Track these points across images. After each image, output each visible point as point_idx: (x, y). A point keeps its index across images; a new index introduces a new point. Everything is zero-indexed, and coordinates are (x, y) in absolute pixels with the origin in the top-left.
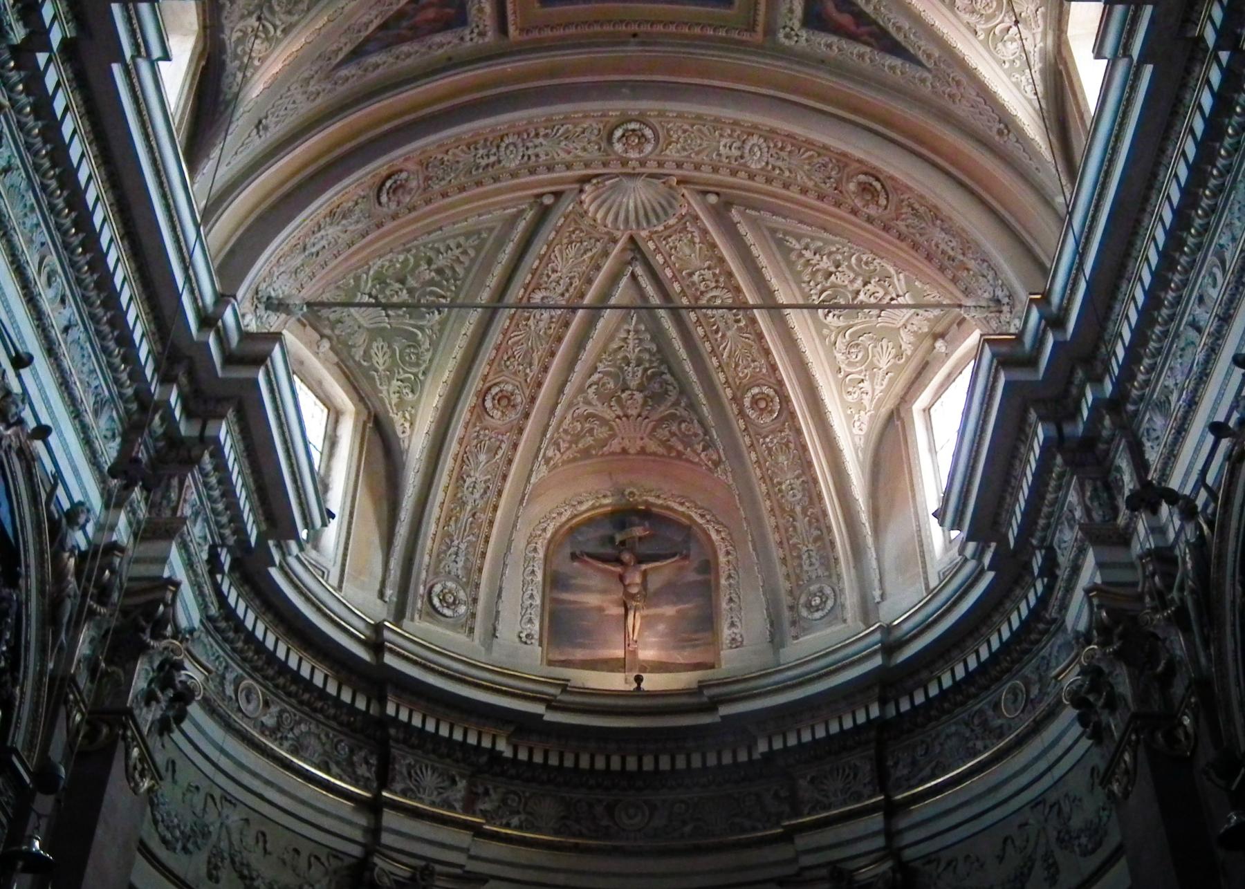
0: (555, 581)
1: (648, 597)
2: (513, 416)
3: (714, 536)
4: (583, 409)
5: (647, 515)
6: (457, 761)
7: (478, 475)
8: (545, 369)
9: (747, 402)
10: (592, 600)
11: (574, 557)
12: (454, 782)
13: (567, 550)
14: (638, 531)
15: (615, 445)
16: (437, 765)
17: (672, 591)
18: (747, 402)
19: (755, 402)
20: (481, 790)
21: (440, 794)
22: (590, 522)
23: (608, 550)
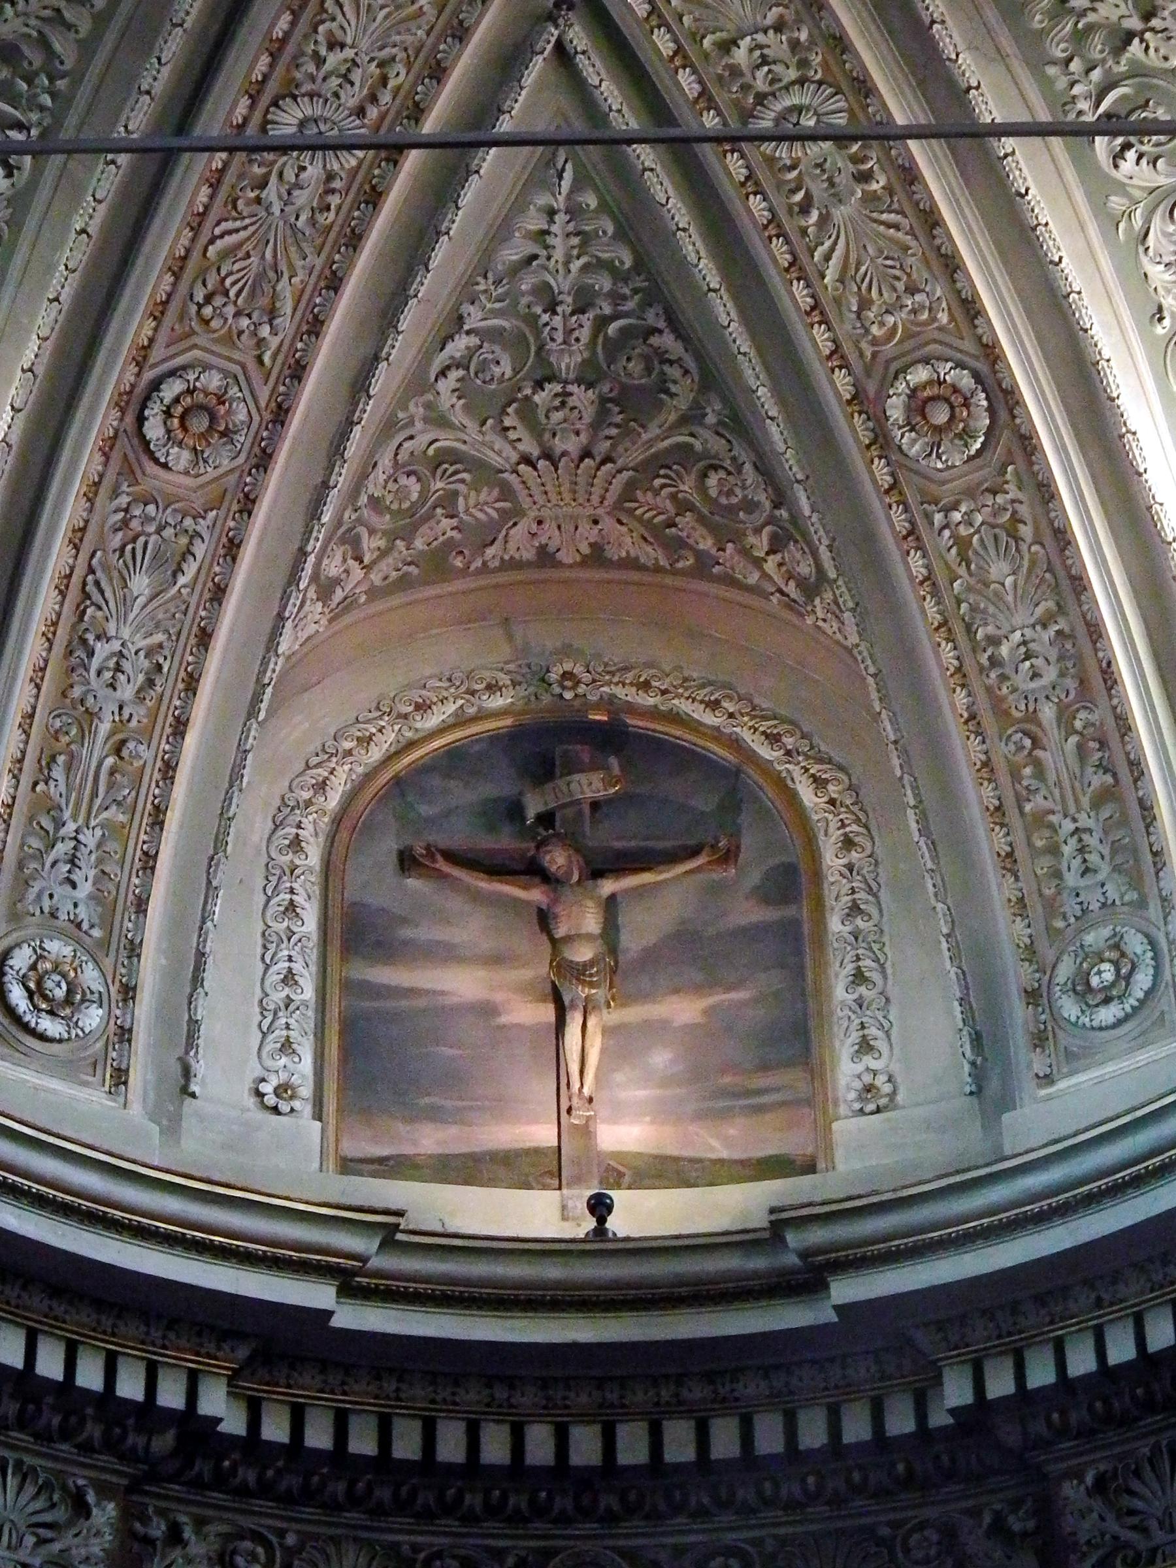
0: (355, 932)
1: (618, 971)
2: (224, 461)
3: (807, 794)
4: (423, 438)
5: (611, 738)
6: (86, 1448)
7: (127, 635)
8: (315, 326)
9: (896, 409)
10: (462, 984)
11: (407, 862)
12: (81, 1509)
13: (388, 845)
14: (589, 786)
15: (519, 541)
16: (29, 1460)
17: (692, 954)
18: (896, 409)
19: (918, 404)
20: (158, 1529)
21: (41, 1542)
22: (454, 761)
23: (505, 841)
